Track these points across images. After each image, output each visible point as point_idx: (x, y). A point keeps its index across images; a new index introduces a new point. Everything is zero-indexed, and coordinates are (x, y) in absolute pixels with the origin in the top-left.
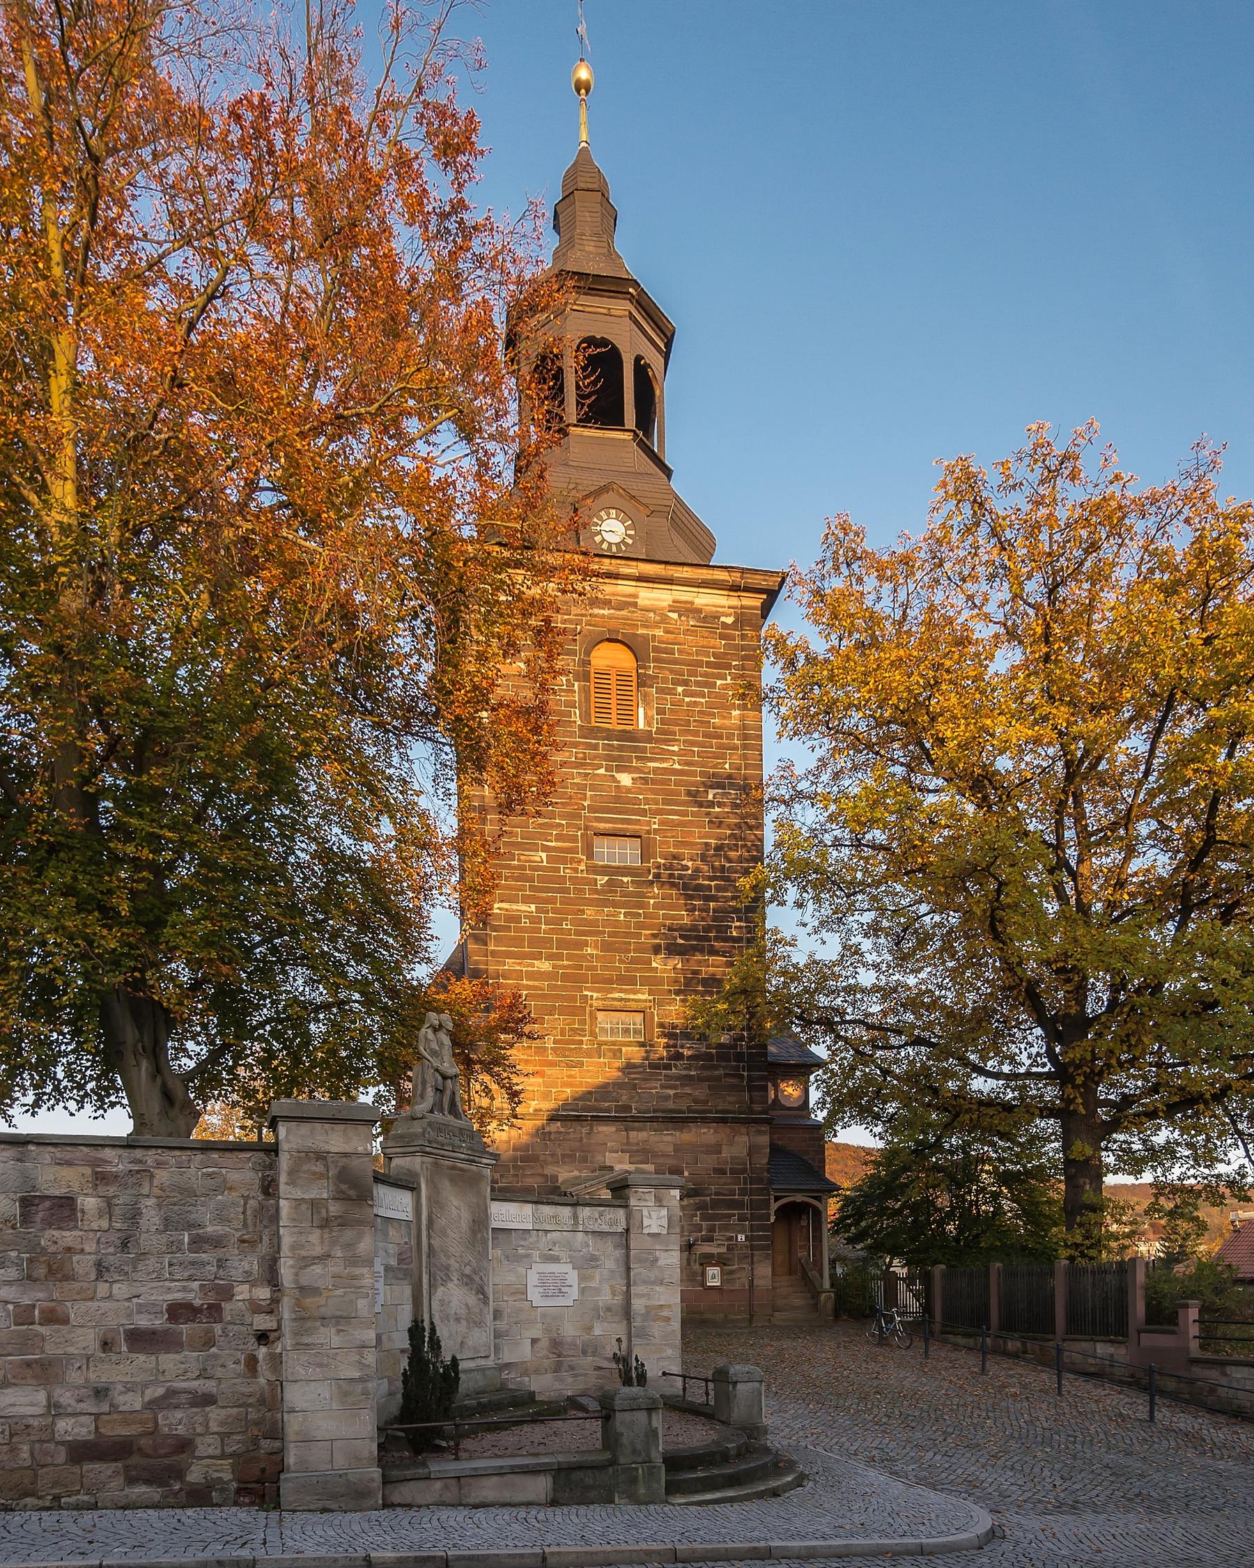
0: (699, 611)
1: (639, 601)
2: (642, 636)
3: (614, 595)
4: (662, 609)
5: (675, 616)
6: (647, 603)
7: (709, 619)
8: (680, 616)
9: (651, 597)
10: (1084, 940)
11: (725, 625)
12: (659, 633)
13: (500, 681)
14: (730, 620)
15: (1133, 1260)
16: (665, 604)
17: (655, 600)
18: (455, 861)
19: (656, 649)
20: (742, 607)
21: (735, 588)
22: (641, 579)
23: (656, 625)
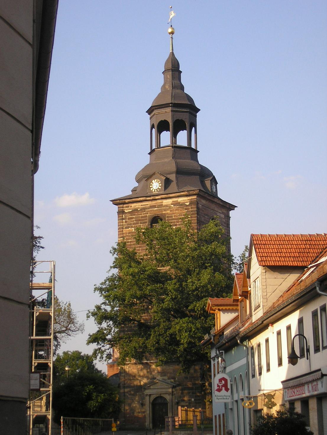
0: (179, 203)
1: (163, 204)
2: (164, 214)
3: (156, 203)
4: (169, 204)
5: (173, 206)
6: (165, 204)
7: (182, 205)
8: (174, 206)
9: (166, 202)
10: (190, 245)
11: (187, 206)
12: (168, 212)
13: (170, 390)
14: (188, 204)
15: (205, 381)
16: (170, 203)
17: (167, 202)
18: (67, 331)
19: (168, 217)
20: (191, 199)
21: (187, 196)
22: (162, 199)
23: (168, 210)
